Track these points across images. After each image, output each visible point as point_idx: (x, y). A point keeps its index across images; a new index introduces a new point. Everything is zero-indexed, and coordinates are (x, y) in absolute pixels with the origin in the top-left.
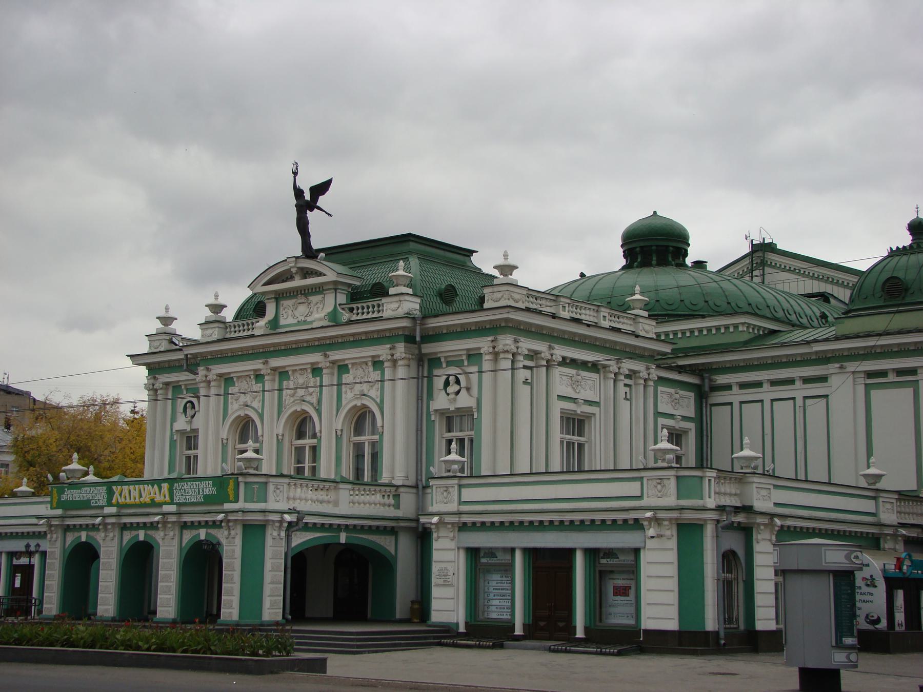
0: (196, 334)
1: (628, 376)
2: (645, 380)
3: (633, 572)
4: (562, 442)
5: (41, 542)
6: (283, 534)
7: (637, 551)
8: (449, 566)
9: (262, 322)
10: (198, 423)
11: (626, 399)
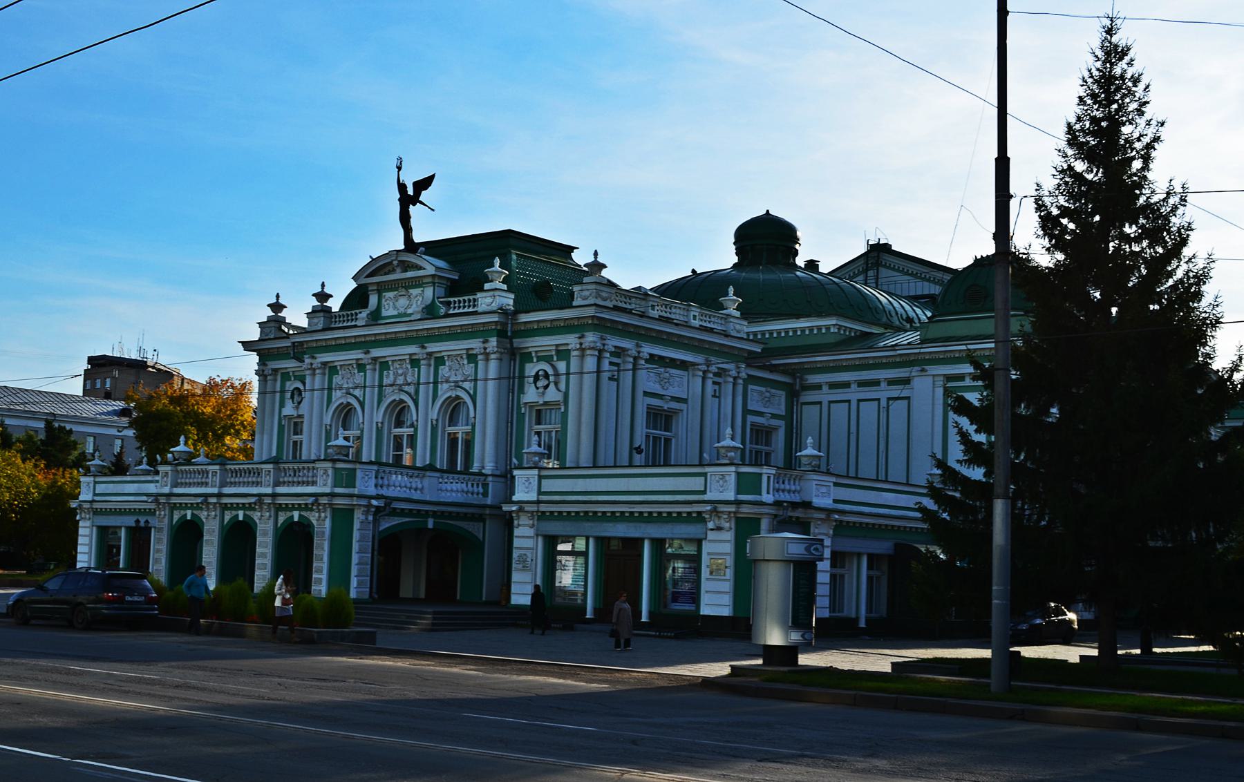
0: (303, 322)
1: (715, 374)
2: (735, 378)
3: (694, 561)
4: (647, 437)
5: (150, 519)
6: (371, 518)
7: (699, 542)
8: (529, 553)
9: (364, 314)
10: (304, 408)
11: (714, 396)
